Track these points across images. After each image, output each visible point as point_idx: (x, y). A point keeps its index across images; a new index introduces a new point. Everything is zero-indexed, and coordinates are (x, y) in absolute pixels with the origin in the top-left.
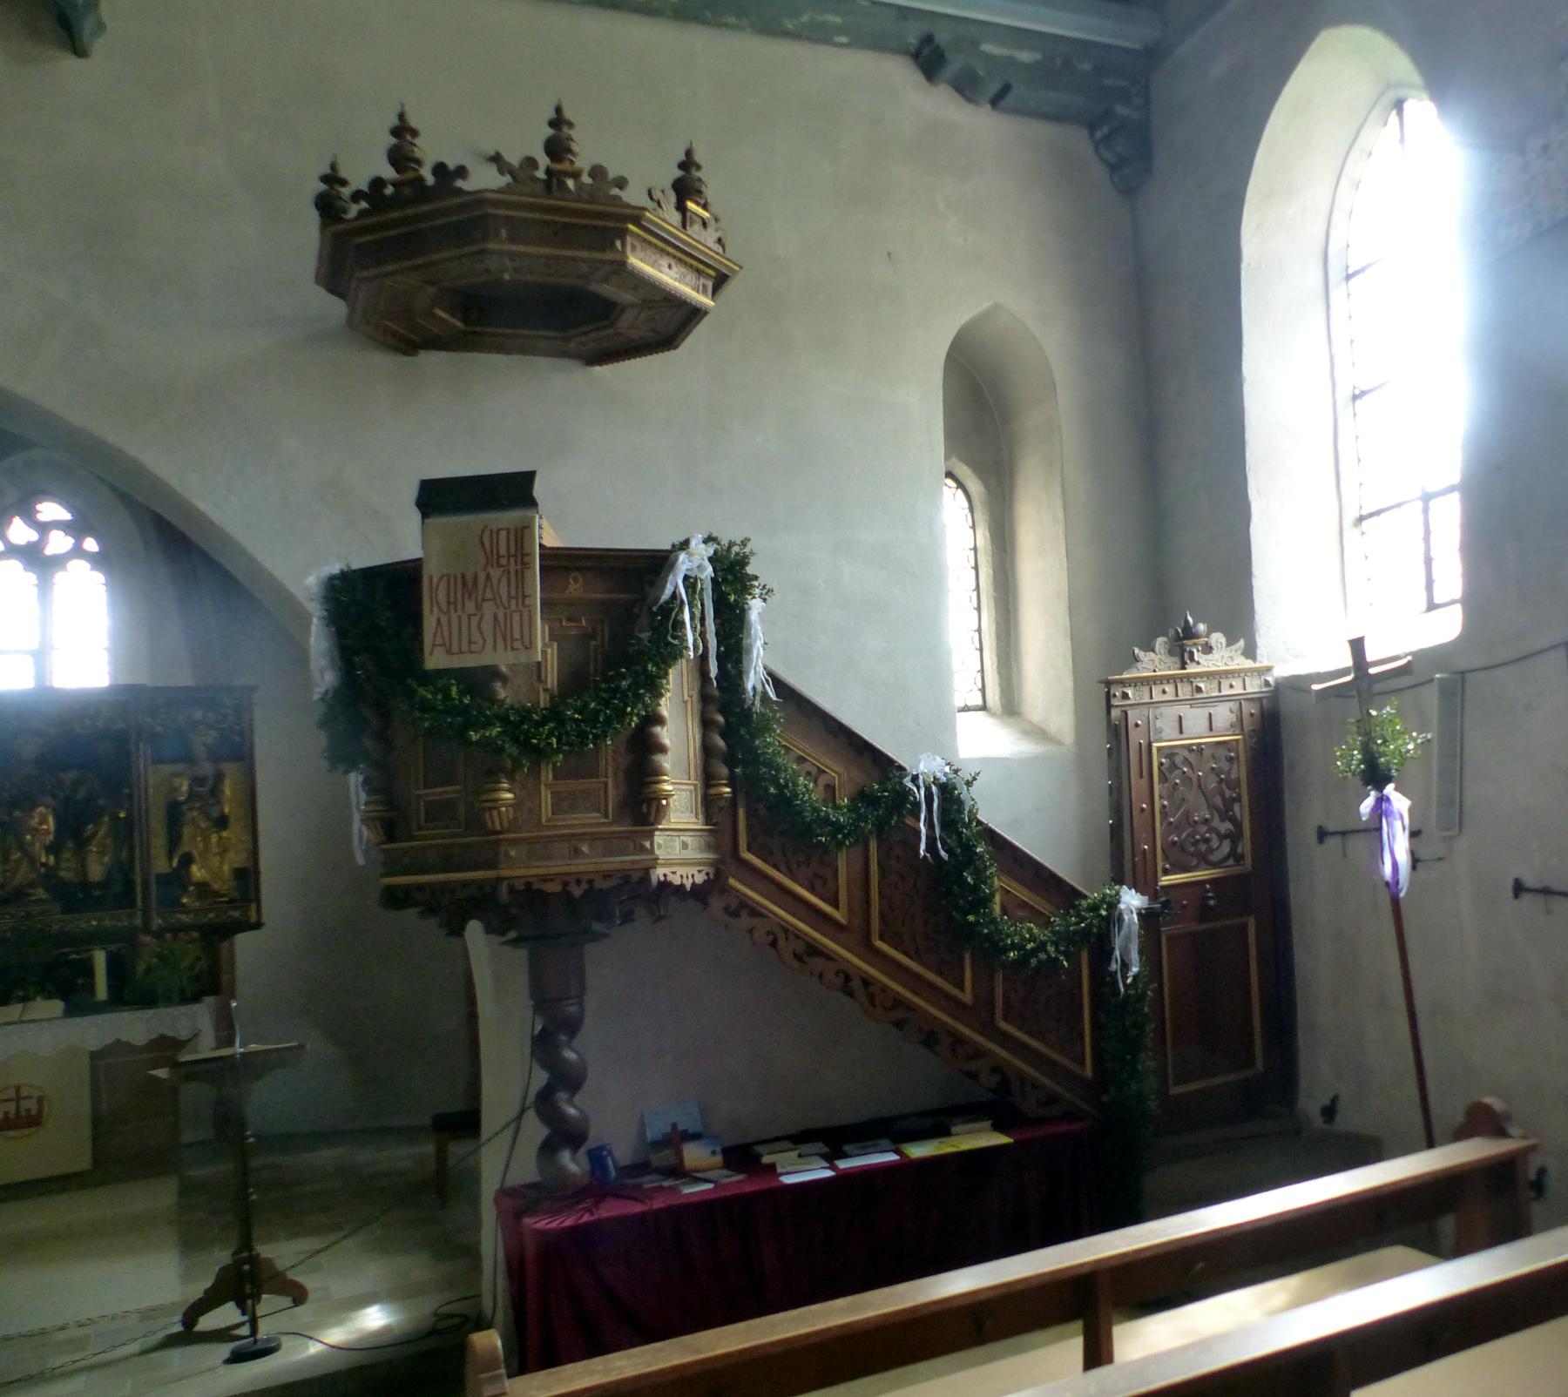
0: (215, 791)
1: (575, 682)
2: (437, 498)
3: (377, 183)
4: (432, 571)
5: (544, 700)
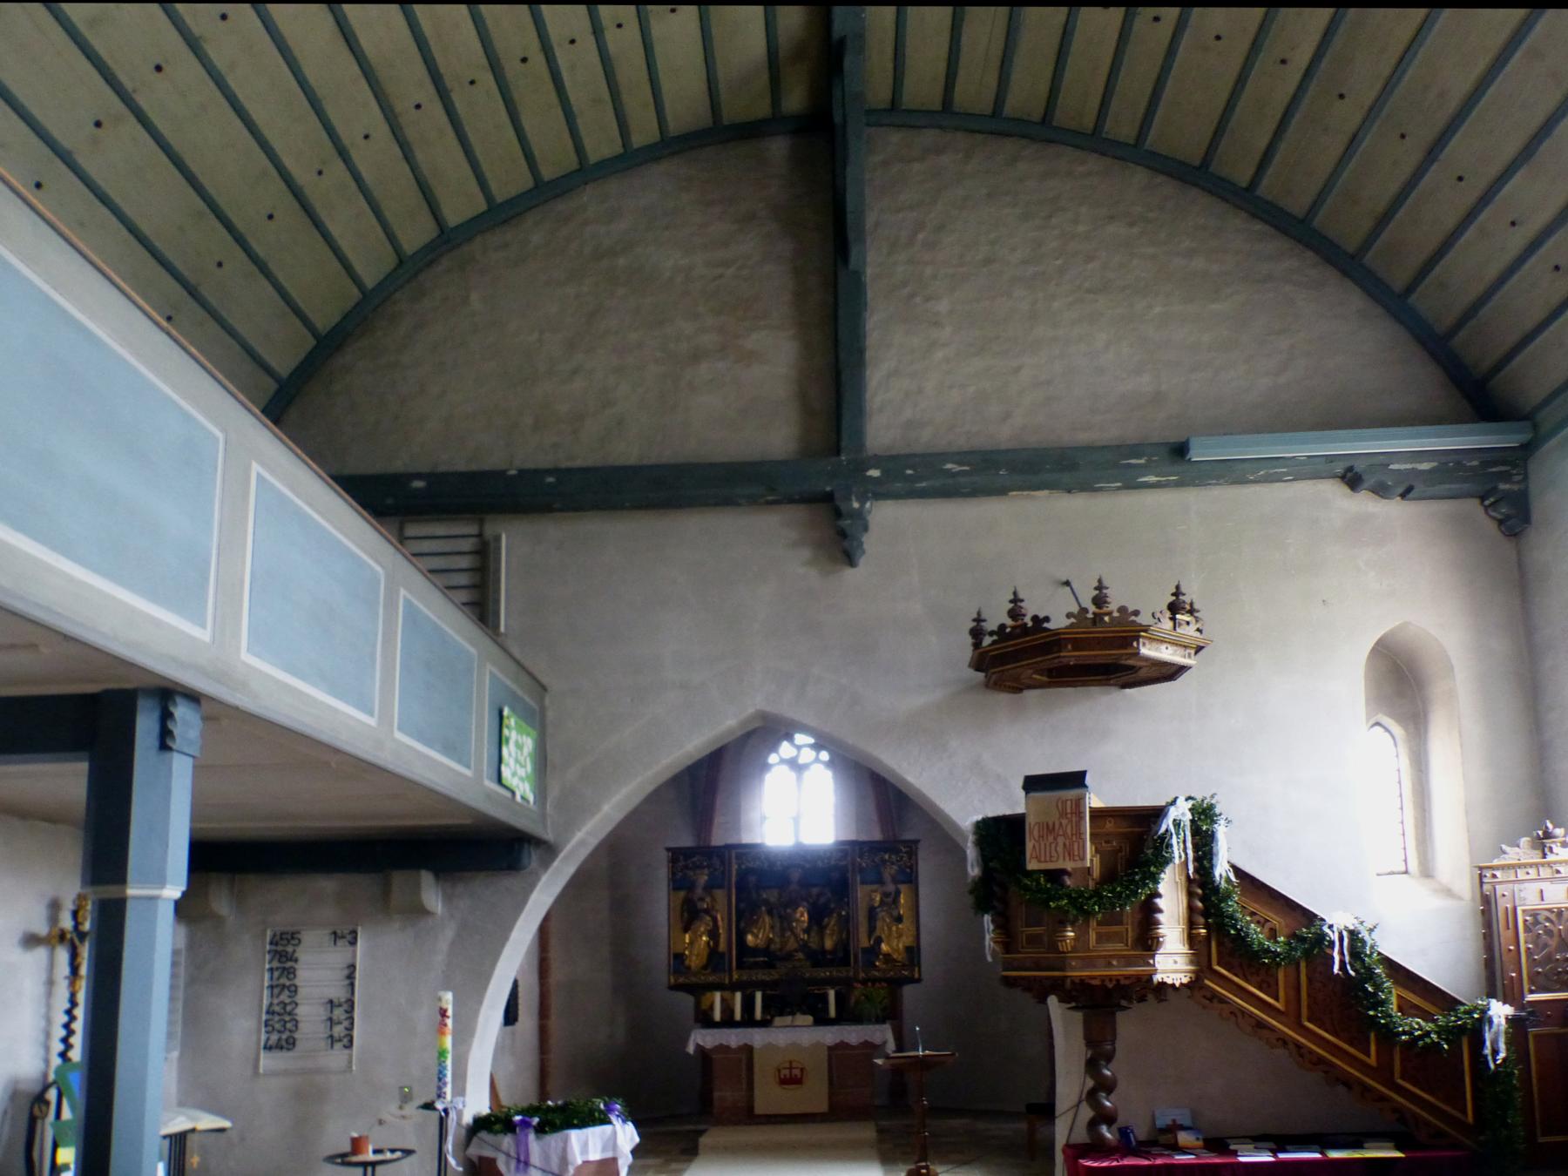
1: (1109, 876)
2: (1033, 784)
3: (1002, 627)
4: (1030, 821)
5: (1091, 885)
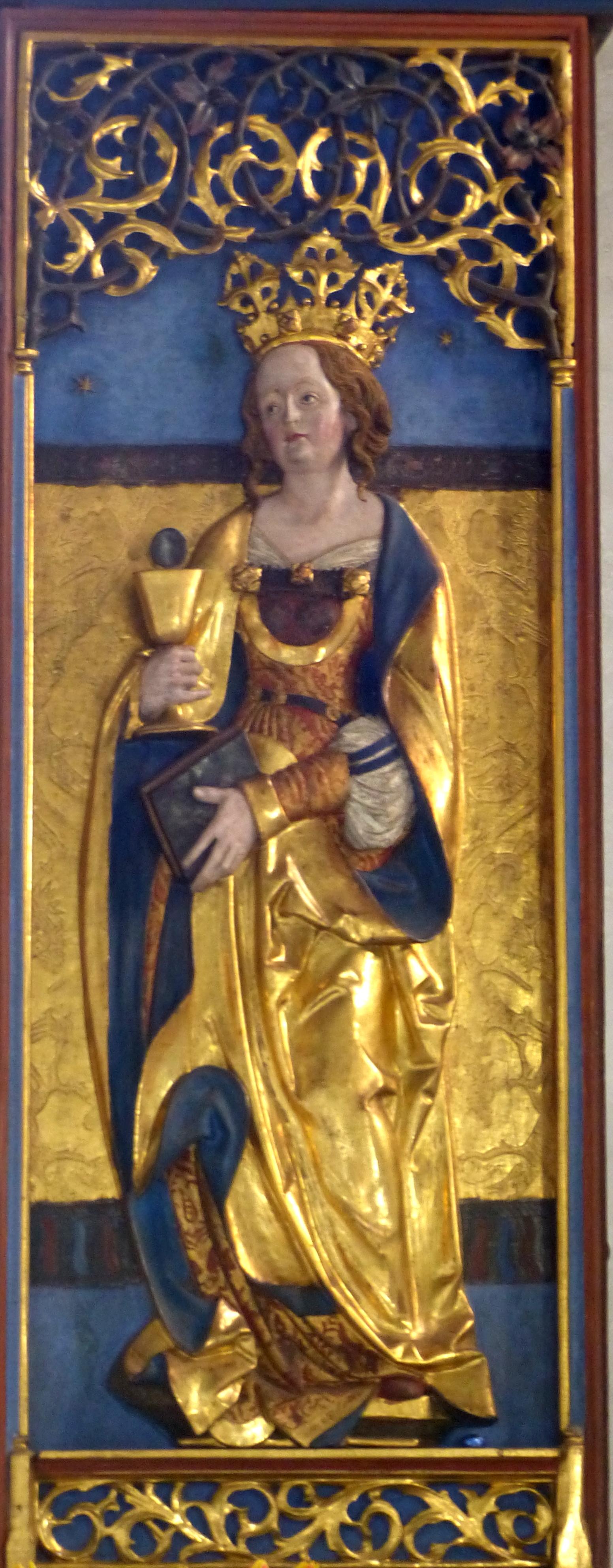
0: (376, 678)
